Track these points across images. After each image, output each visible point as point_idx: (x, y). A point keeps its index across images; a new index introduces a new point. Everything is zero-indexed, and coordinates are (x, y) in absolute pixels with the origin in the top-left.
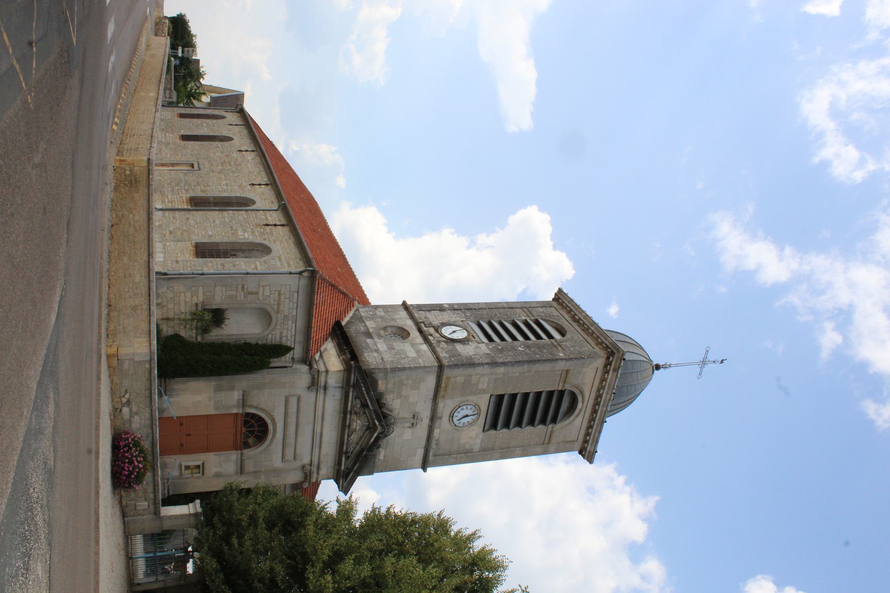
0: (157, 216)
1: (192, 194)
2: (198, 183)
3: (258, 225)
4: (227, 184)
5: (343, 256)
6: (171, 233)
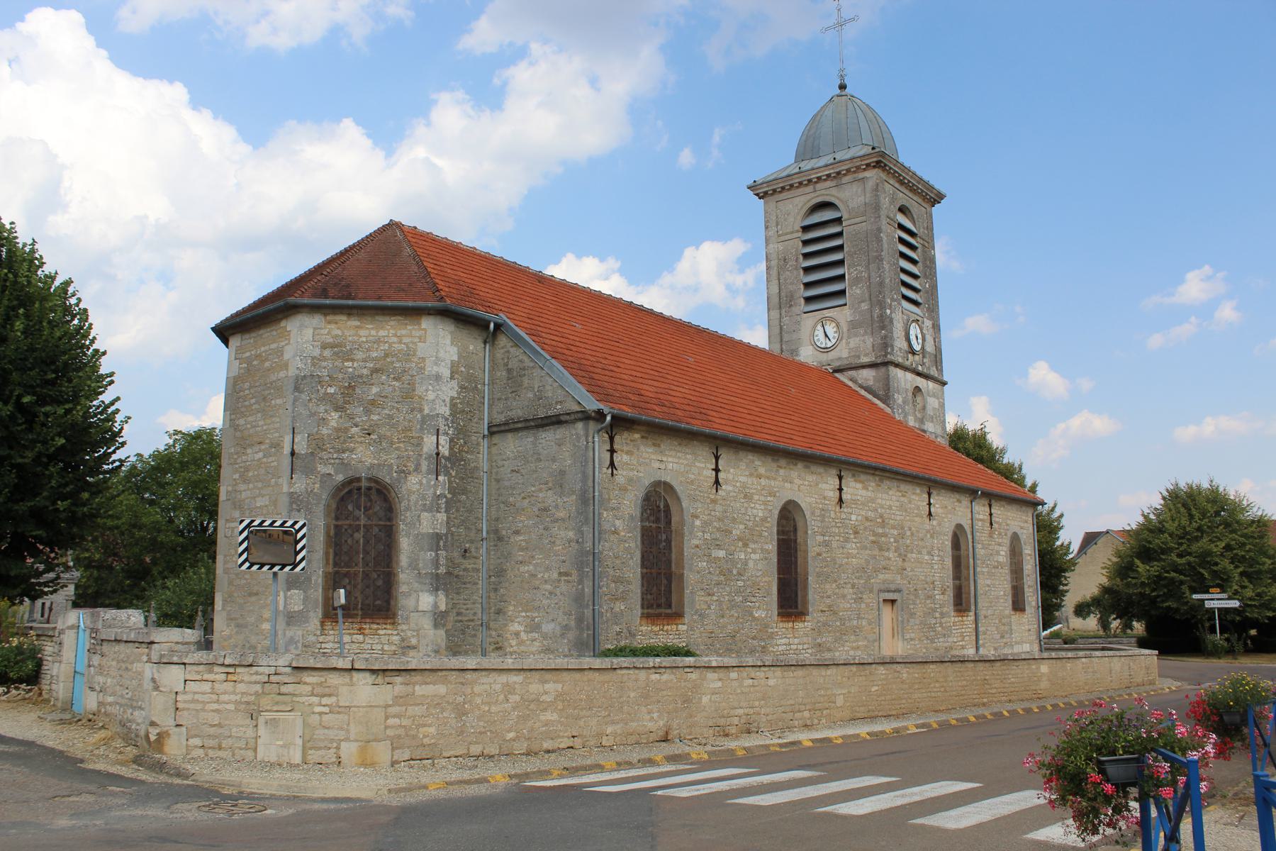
0: (987, 651)
1: (950, 608)
2: (929, 597)
3: (991, 536)
4: (929, 553)
5: (346, 251)
6: (1002, 637)
